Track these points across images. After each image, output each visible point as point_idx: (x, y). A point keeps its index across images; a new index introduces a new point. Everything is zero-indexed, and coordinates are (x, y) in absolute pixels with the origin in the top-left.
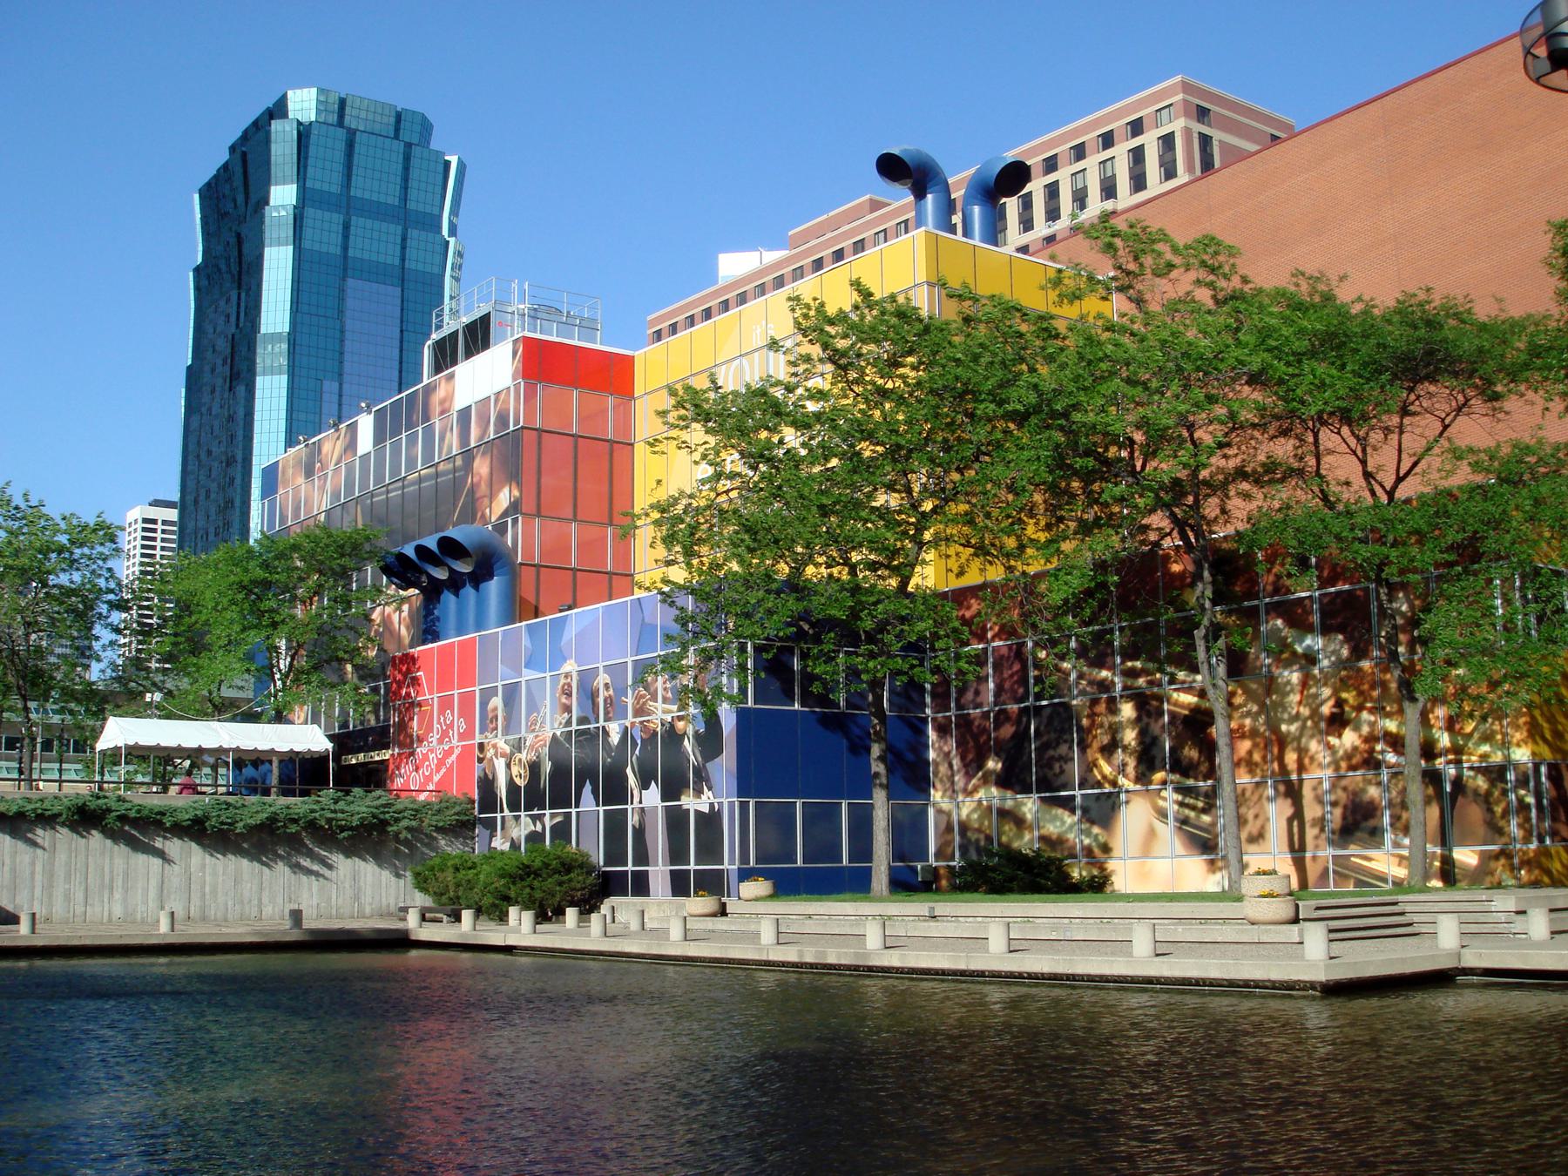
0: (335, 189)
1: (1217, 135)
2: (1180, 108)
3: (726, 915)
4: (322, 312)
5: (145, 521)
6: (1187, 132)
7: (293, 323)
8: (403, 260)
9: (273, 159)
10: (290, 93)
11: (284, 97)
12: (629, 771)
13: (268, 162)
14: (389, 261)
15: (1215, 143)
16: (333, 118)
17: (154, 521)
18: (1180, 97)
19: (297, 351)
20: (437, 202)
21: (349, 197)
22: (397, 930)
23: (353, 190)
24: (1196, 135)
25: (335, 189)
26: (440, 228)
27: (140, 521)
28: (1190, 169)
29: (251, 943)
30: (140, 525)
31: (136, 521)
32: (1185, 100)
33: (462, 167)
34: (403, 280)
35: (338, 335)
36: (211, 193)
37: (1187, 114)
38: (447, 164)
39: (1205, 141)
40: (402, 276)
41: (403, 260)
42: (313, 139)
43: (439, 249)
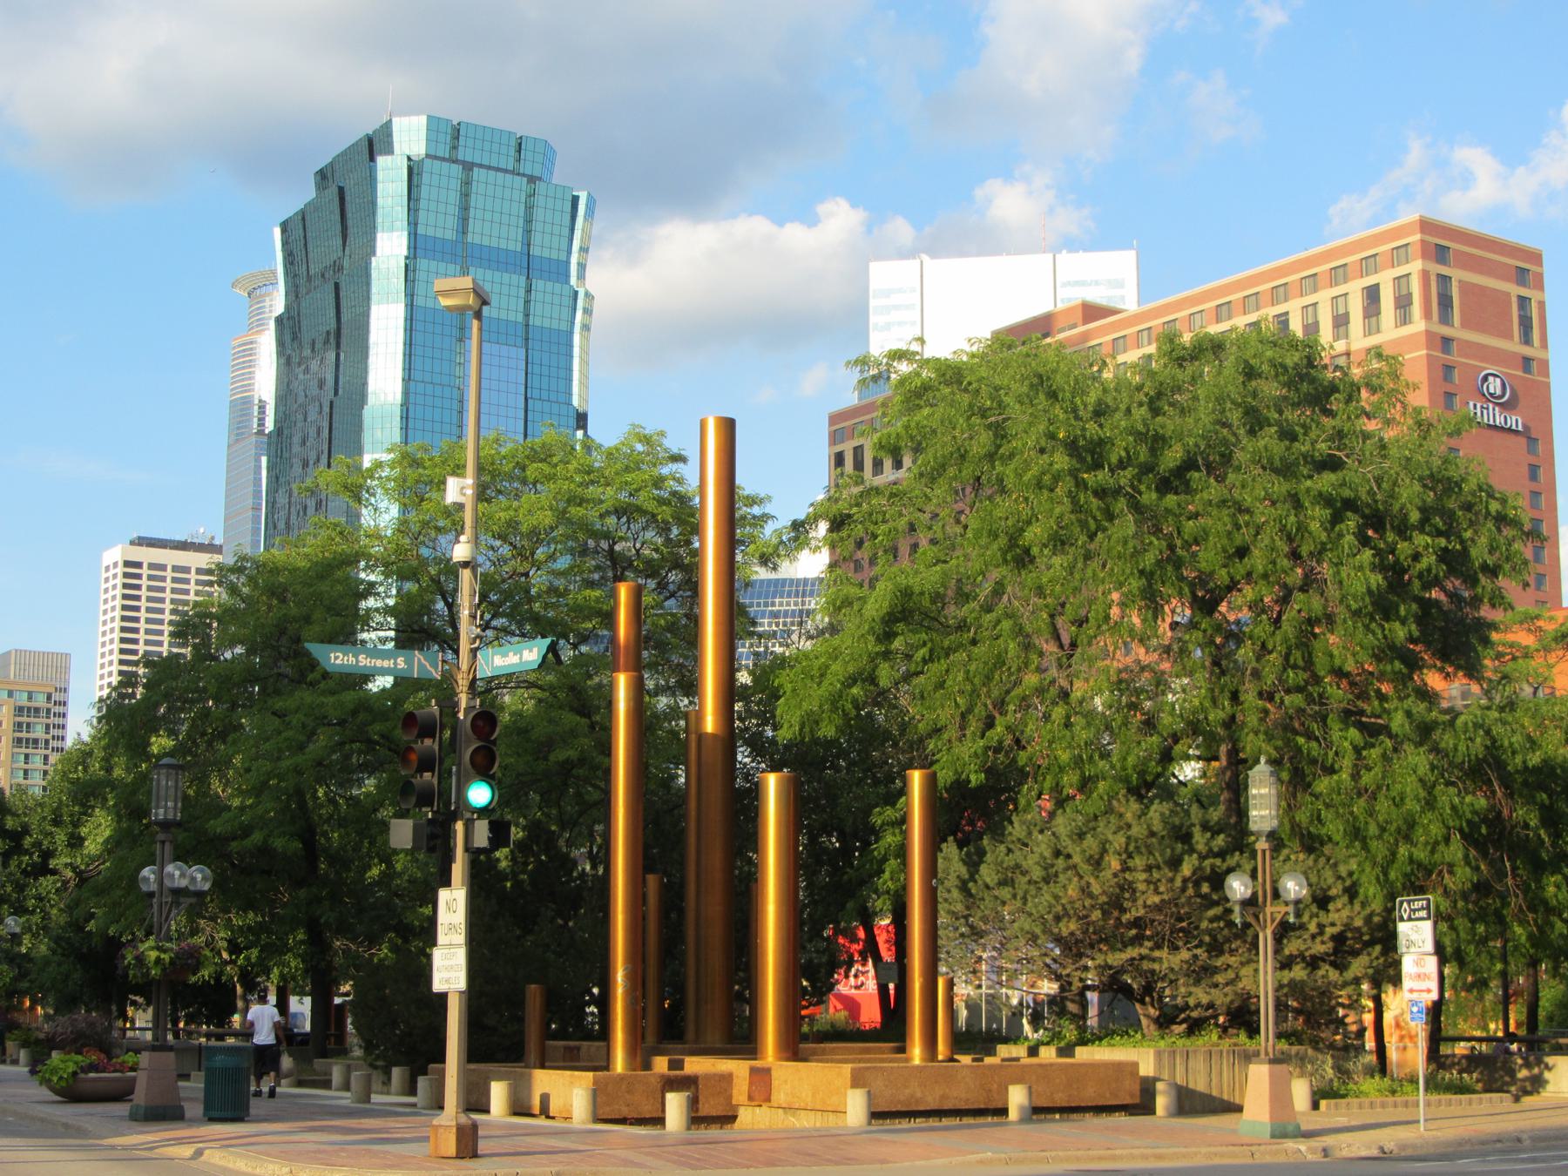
0: (450, 235)
1: (1457, 274)
2: (1418, 248)
3: (475, 1155)
4: (437, 379)
5: (127, 564)
6: (1425, 275)
7: (406, 393)
8: (527, 315)
9: (380, 201)
10: (394, 120)
11: (388, 125)
12: (1025, 1021)
13: (373, 203)
14: (512, 317)
15: (1454, 283)
16: (443, 151)
17: (139, 565)
18: (1418, 237)
19: (411, 425)
20: (564, 246)
21: (464, 243)
22: (1426, 1051)
23: (470, 236)
24: (1433, 279)
25: (450, 235)
26: (568, 276)
27: (121, 564)
28: (1427, 315)
29: (365, 1117)
30: (120, 570)
31: (115, 565)
32: (1422, 241)
33: (590, 199)
34: (527, 339)
35: (456, 406)
36: (297, 233)
37: (1425, 255)
38: (575, 200)
39: (1444, 280)
40: (526, 333)
41: (527, 315)
42: (426, 178)
43: (567, 301)
